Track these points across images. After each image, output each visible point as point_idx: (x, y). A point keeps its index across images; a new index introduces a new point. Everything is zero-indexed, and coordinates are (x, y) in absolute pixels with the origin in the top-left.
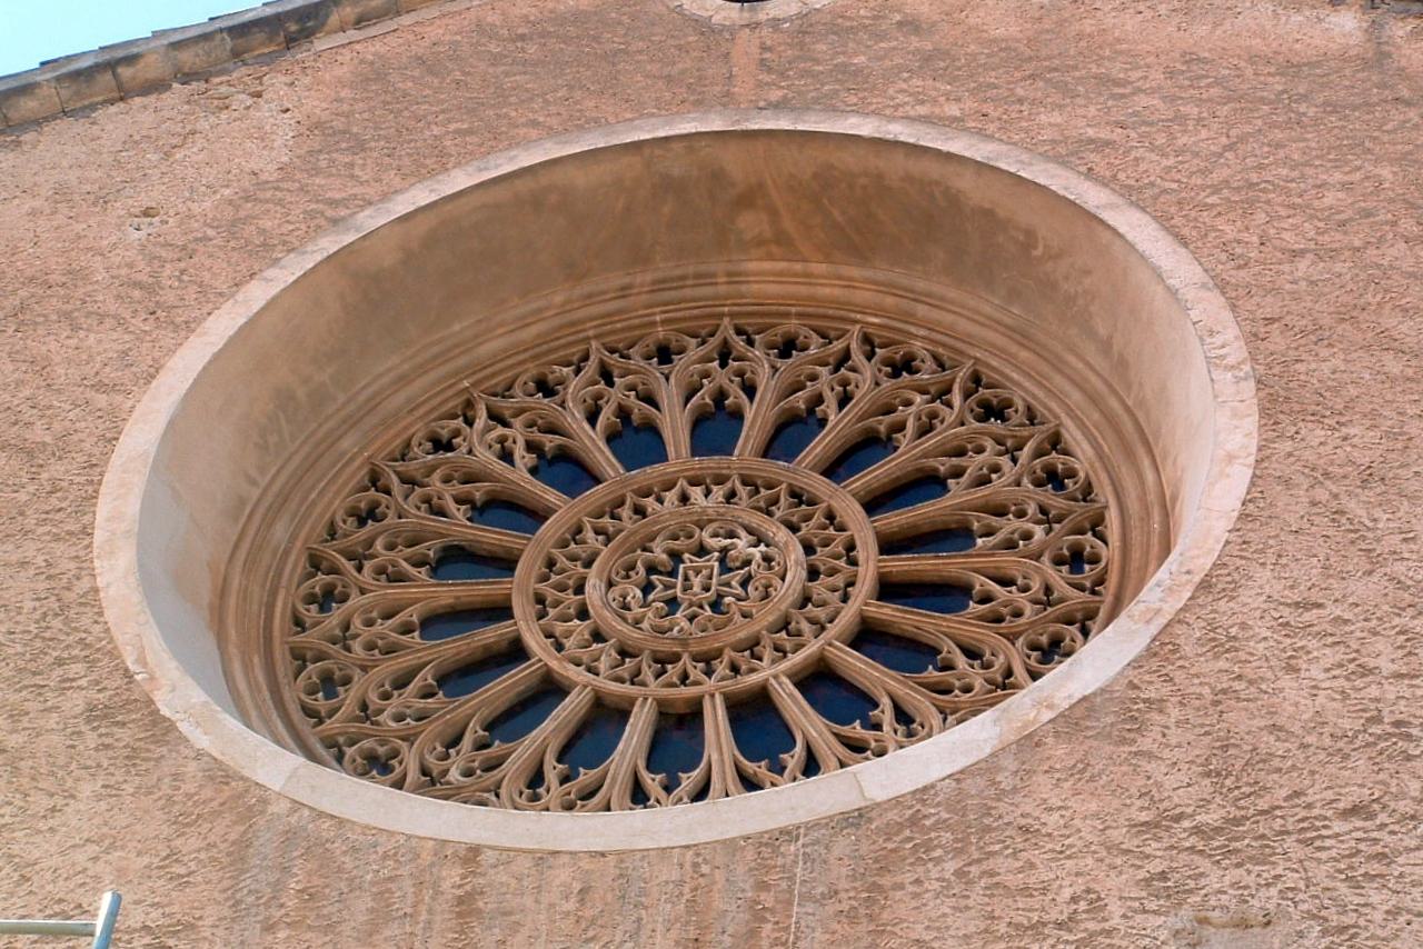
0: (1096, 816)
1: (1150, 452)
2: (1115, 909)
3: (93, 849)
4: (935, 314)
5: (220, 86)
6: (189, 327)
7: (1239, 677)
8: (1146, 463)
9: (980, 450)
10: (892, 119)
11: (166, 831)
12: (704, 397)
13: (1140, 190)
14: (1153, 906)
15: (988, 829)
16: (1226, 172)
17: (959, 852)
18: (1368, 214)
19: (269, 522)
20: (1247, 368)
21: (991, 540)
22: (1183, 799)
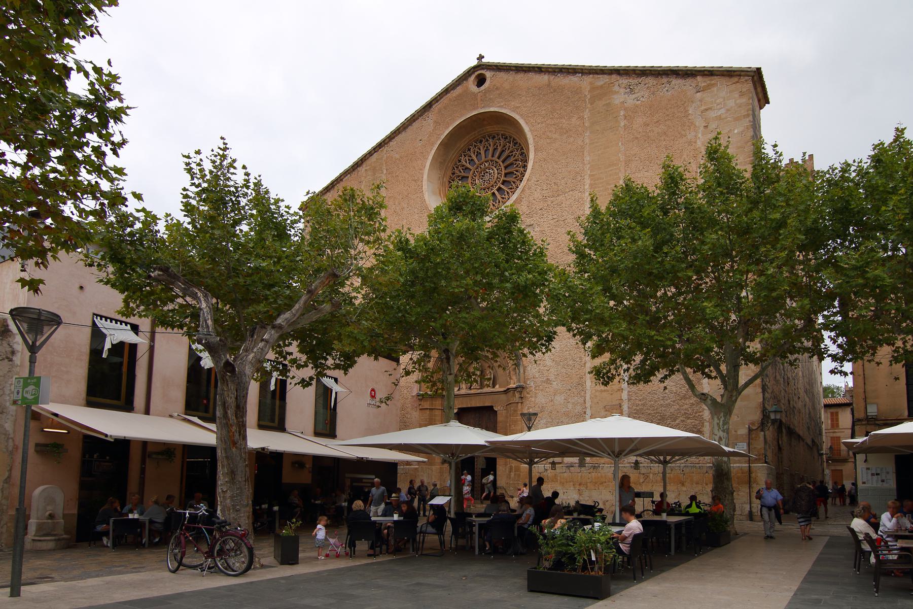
19: (443, 179)
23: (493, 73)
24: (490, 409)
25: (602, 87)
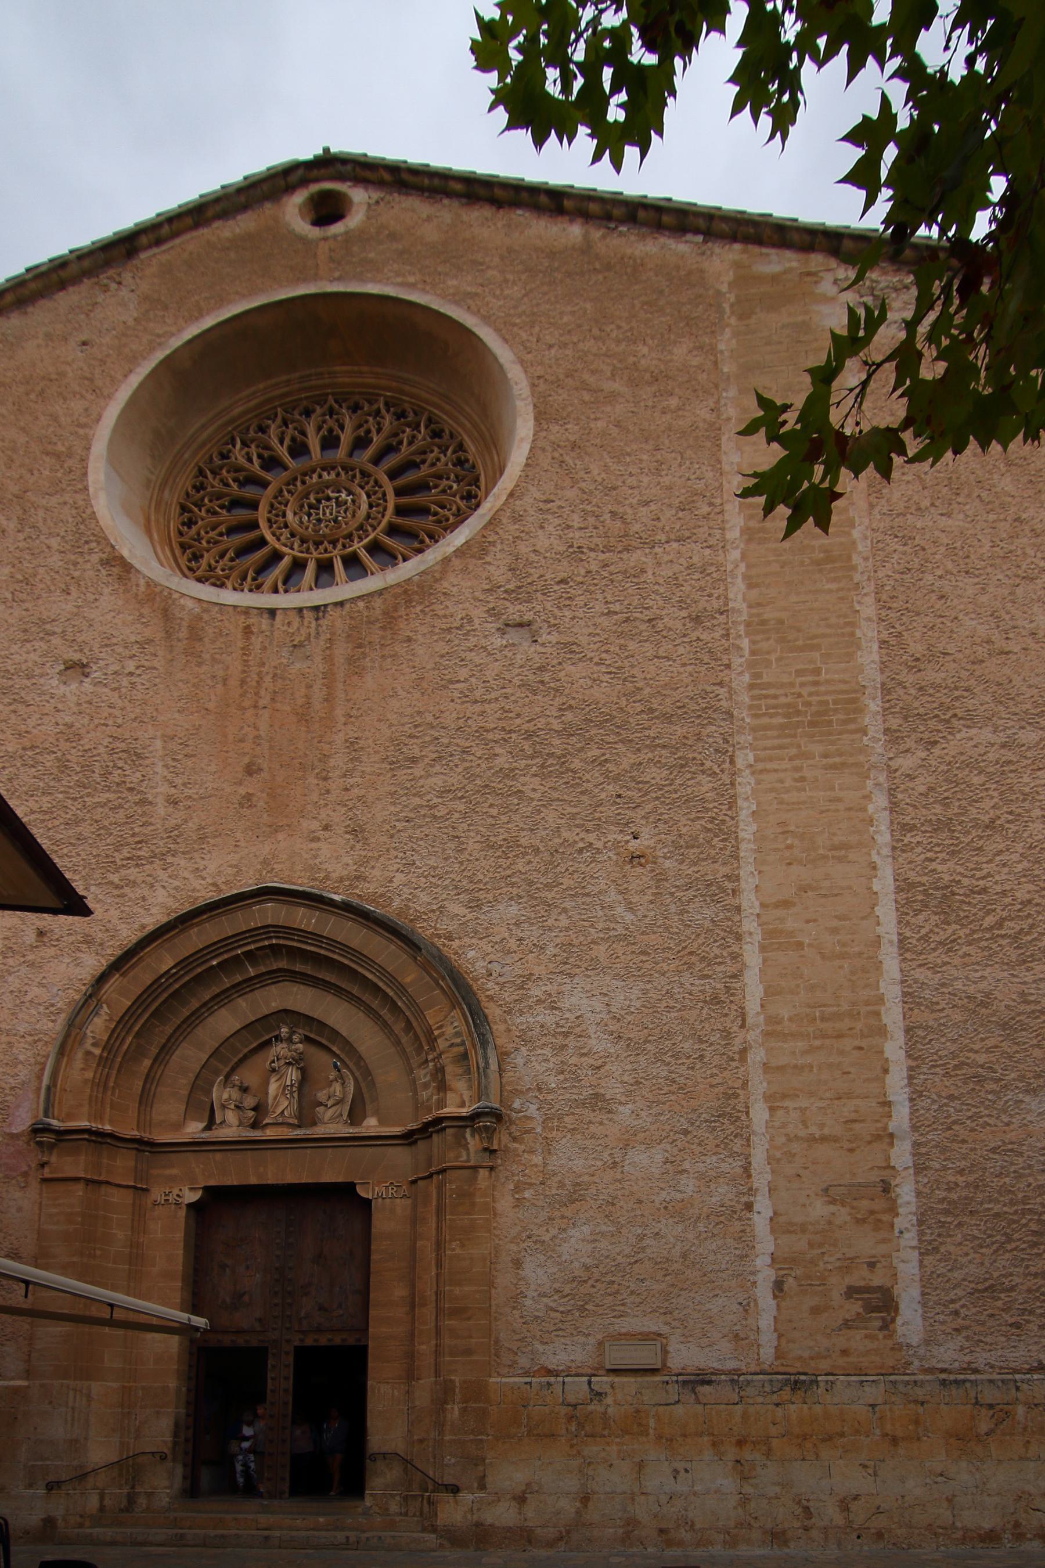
0: (470, 587)
1: (496, 447)
2: (477, 621)
3: (113, 614)
4: (415, 391)
5: (103, 278)
6: (110, 397)
7: (523, 531)
8: (494, 452)
9: (432, 451)
10: (387, 284)
11: (137, 606)
12: (324, 432)
13: (489, 317)
14: (490, 620)
15: (432, 594)
16: (524, 307)
17: (421, 603)
18: (579, 326)
20: (530, 399)
21: (437, 490)
22: (502, 580)
23: (376, 195)
24: (346, 1191)
25: (775, 278)
